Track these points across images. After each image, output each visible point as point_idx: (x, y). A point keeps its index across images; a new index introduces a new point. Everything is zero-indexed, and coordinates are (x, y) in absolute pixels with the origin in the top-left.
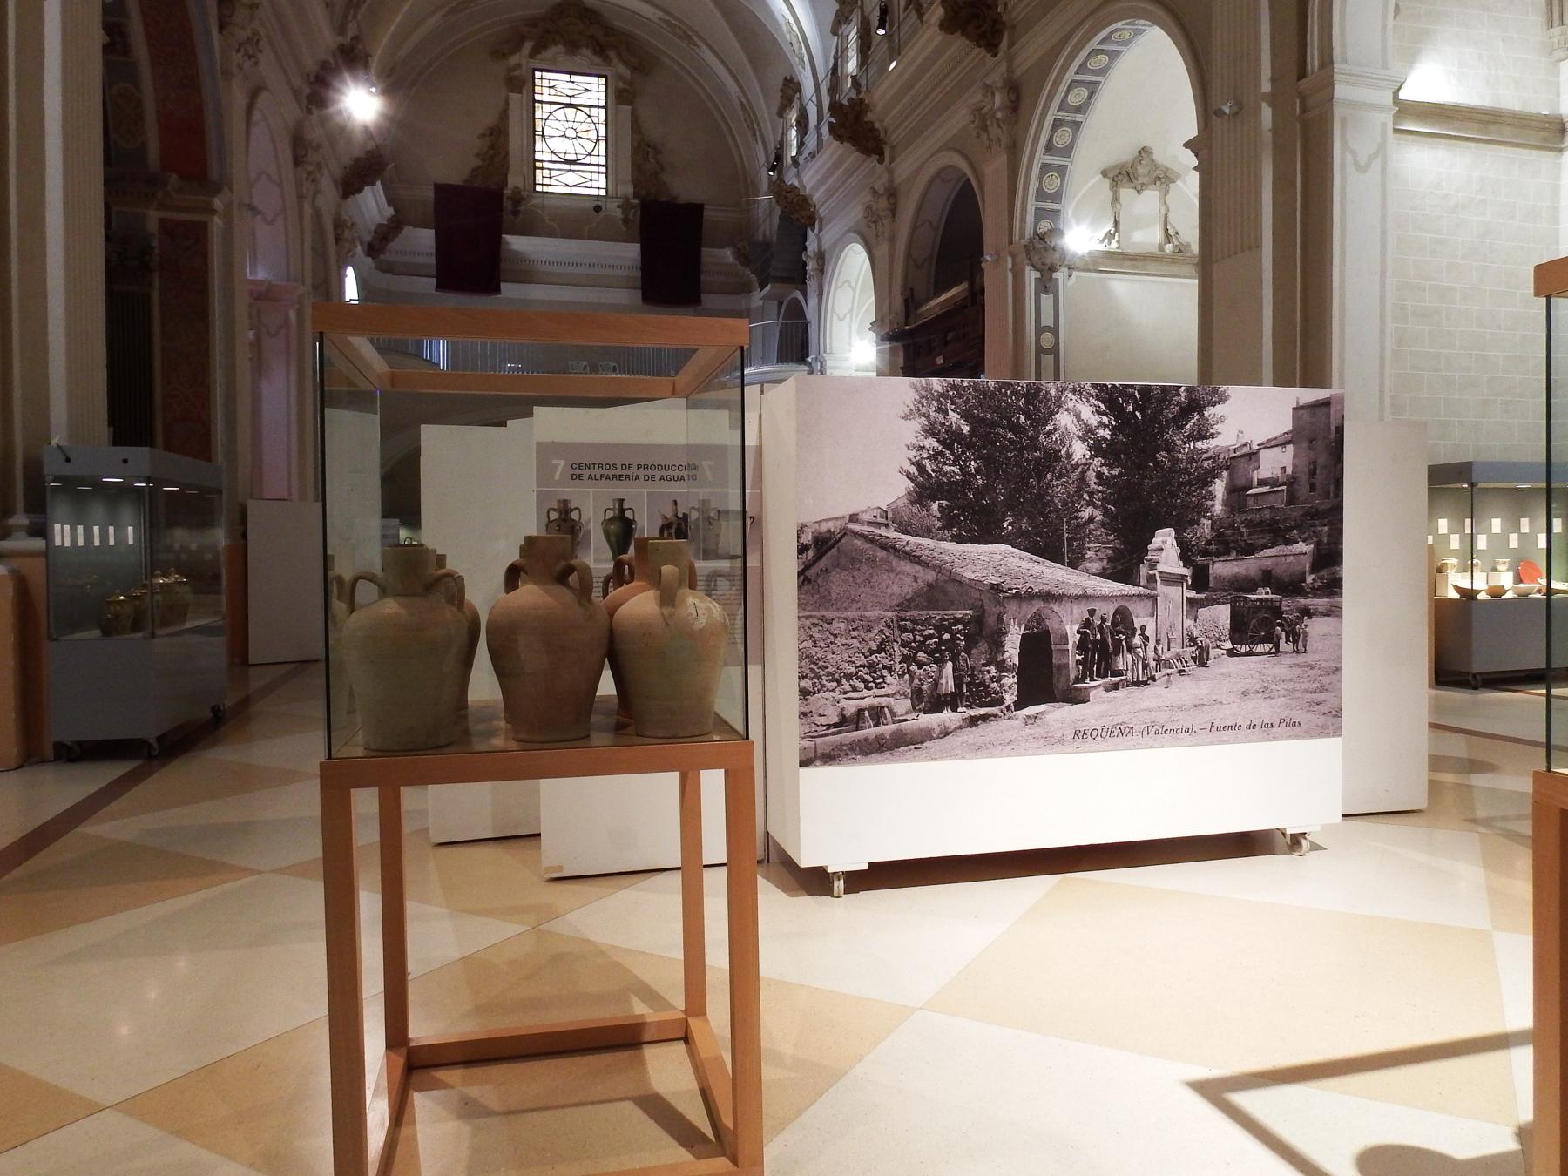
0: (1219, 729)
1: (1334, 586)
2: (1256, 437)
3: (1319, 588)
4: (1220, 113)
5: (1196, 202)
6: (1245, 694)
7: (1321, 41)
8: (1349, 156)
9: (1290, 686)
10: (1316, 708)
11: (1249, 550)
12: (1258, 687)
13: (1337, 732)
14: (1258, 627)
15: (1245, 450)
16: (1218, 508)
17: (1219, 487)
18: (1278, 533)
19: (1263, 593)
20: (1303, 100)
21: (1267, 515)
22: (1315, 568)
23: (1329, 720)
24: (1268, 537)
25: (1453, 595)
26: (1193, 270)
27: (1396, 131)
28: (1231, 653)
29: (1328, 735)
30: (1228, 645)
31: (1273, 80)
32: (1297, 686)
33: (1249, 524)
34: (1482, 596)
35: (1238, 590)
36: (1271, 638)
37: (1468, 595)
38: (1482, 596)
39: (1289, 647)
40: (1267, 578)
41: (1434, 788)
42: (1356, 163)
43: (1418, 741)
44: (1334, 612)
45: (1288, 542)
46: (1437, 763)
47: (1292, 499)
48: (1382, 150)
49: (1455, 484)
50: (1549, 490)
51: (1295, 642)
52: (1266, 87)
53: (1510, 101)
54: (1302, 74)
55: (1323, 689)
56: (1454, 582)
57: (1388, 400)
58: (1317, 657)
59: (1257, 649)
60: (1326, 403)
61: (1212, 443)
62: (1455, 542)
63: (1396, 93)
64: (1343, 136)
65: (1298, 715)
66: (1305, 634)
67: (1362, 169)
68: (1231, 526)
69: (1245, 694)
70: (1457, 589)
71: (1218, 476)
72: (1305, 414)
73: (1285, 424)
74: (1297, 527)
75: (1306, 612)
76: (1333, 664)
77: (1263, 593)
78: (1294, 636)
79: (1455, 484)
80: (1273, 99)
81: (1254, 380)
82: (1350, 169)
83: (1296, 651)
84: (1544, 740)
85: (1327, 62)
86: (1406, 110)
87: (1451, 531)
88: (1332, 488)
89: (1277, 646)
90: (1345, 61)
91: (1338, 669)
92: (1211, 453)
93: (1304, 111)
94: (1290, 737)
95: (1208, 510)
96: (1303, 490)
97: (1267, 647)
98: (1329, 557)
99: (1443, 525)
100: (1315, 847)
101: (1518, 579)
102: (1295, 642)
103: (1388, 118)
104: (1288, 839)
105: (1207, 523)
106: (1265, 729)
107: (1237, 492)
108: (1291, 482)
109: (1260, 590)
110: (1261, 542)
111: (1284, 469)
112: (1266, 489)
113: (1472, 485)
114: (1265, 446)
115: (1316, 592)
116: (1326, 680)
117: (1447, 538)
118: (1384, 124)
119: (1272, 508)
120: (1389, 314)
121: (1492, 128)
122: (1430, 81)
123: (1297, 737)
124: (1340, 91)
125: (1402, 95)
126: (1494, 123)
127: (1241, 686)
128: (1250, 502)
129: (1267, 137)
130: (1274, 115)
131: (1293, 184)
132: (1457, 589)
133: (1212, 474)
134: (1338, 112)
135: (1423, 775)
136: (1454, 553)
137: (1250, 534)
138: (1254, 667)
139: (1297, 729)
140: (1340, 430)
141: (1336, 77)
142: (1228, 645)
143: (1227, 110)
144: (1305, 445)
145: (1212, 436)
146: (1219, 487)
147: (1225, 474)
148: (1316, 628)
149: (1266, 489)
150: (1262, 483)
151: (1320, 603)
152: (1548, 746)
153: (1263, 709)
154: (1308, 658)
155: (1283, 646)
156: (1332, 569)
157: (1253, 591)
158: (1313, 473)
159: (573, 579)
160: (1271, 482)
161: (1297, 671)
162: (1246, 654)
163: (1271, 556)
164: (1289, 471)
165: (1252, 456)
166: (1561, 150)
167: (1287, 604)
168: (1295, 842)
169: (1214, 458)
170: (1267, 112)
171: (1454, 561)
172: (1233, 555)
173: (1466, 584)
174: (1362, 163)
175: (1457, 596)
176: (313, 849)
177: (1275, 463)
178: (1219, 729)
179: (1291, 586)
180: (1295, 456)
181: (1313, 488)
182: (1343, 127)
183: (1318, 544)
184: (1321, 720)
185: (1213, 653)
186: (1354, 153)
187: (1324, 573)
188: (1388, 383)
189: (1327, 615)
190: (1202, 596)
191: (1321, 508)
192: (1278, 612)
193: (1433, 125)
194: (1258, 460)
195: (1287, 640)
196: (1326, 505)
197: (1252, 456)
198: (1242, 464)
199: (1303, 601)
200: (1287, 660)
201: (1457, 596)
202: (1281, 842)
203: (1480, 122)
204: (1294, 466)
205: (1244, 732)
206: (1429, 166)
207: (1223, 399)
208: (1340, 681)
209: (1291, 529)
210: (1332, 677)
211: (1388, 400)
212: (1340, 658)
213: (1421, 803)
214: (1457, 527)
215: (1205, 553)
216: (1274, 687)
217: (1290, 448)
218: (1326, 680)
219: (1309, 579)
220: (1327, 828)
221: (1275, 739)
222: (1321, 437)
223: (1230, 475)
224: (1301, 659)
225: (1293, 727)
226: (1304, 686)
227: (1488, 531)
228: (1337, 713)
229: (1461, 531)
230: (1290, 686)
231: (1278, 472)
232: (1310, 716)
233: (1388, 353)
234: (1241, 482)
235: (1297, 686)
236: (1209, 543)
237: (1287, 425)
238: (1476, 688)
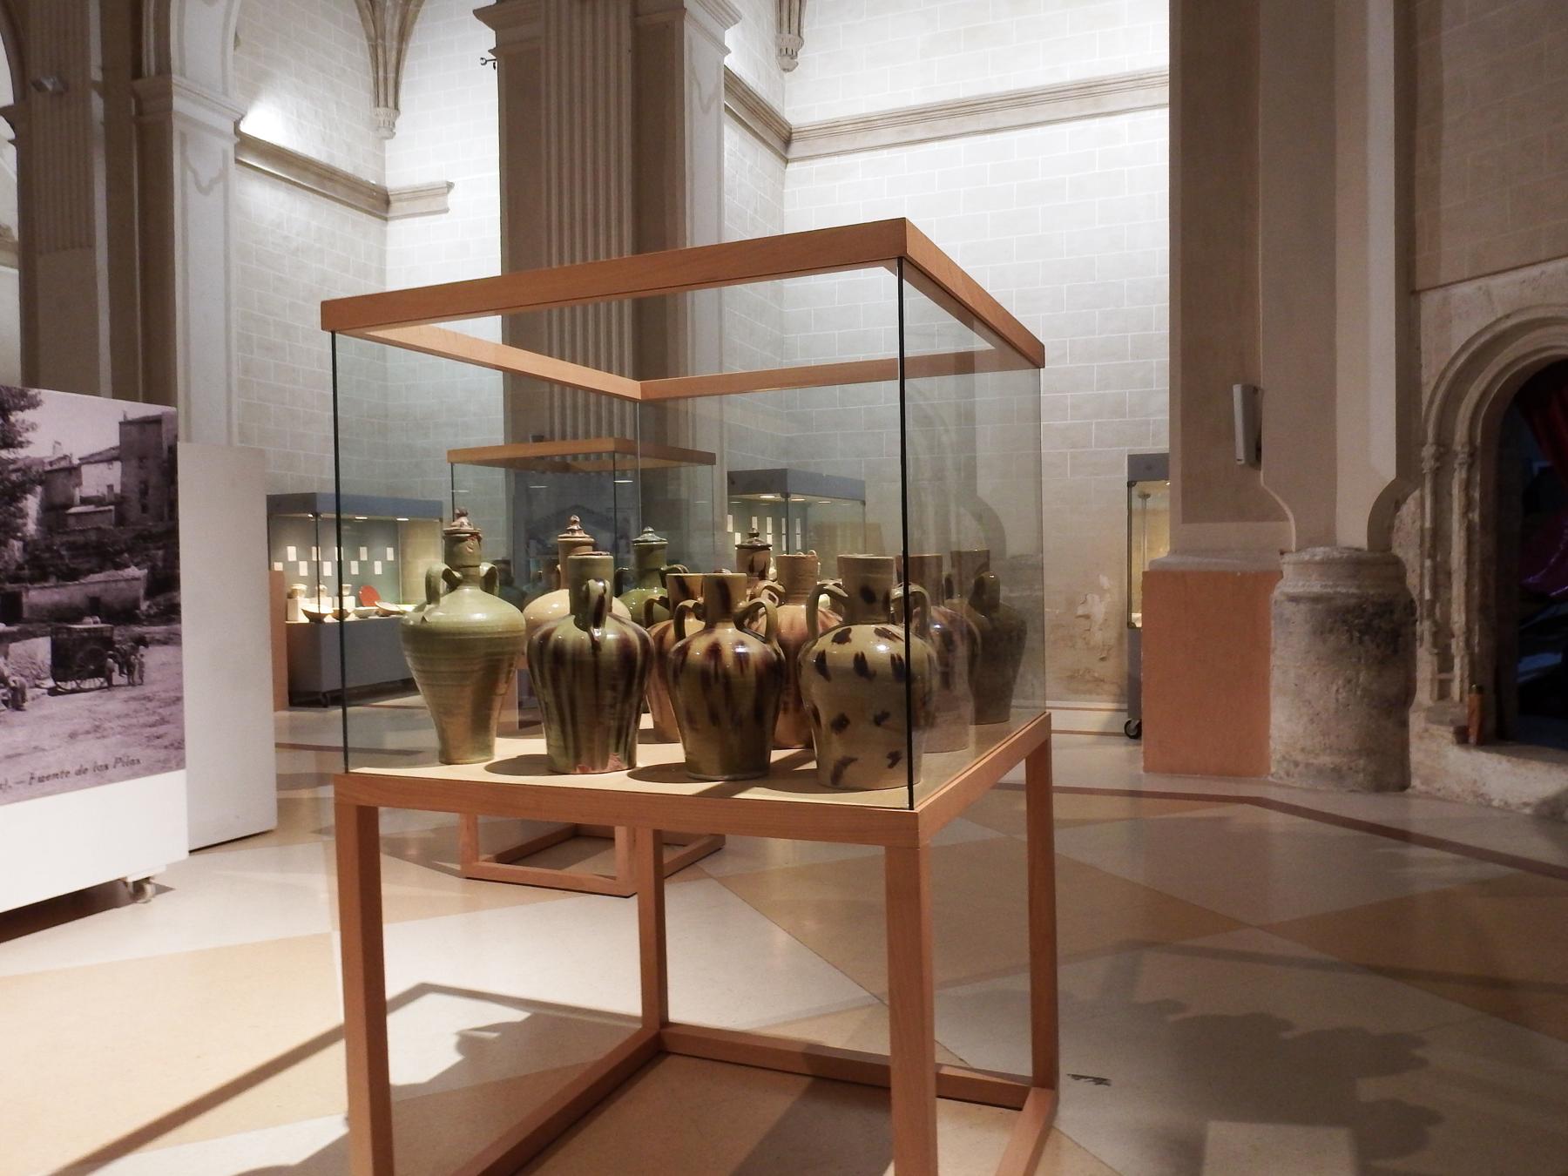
0: (41, 780)
1: (171, 613)
2: (77, 449)
3: (155, 615)
4: (40, 87)
5: (15, 178)
6: (73, 736)
7: (157, 48)
8: (189, 174)
9: (126, 722)
10: (157, 742)
11: (72, 575)
12: (87, 727)
13: (180, 764)
14: (79, 662)
15: (63, 464)
16: (31, 527)
17: (32, 504)
18: (105, 555)
19: (90, 623)
20: (139, 103)
21: (93, 536)
22: (149, 594)
23: (171, 753)
24: (94, 562)
25: (304, 620)
26: (14, 259)
27: (238, 162)
28: (53, 692)
29: (171, 769)
30: (50, 683)
31: (104, 69)
32: (134, 721)
33: (71, 546)
34: (329, 619)
35: (59, 620)
36: (102, 672)
37: (316, 619)
38: (329, 619)
39: (124, 680)
40: (95, 606)
41: (286, 809)
42: (198, 183)
43: (264, 763)
44: (173, 640)
45: (119, 567)
46: (286, 782)
47: (121, 520)
48: (223, 176)
49: (288, 513)
50: (339, 521)
51: (130, 673)
52: (96, 75)
53: (343, 163)
54: (137, 73)
55: (163, 721)
56: (304, 607)
57: (235, 429)
58: (155, 688)
59: (87, 684)
60: (157, 421)
61: (21, 453)
62: (303, 569)
63: (237, 124)
64: (183, 153)
65: (136, 752)
66: (142, 665)
67: (205, 191)
68: (49, 548)
69: (73, 736)
70: (307, 614)
71: (31, 491)
72: (134, 430)
73: (111, 439)
74: (130, 550)
75: (142, 641)
76: (172, 694)
77: (90, 623)
78: (128, 667)
79: (288, 513)
80: (105, 92)
81: (88, 386)
82: (191, 189)
83: (132, 684)
84: (341, 744)
85: (164, 69)
86: (247, 144)
87: (299, 558)
88: (166, 510)
89: (109, 680)
90: (183, 74)
91: (179, 699)
92: (20, 464)
93: (140, 112)
94: (128, 777)
95: (18, 529)
96: (134, 512)
97: (98, 682)
98: (165, 582)
99: (292, 552)
100: (161, 890)
101: (359, 603)
102: (130, 673)
103: (229, 146)
104: (131, 888)
105: (17, 544)
106: (98, 773)
107: (54, 511)
108: (120, 501)
109: (88, 620)
110: (87, 566)
111: (110, 487)
112: (91, 508)
113: (316, 515)
114: (89, 460)
115: (151, 619)
116: (165, 712)
117: (295, 565)
118: (225, 153)
119: (98, 529)
120: (234, 343)
121: (329, 184)
122: (267, 121)
123: (136, 775)
124: (178, 103)
125: (245, 128)
126: (331, 180)
127: (68, 728)
128: (71, 521)
129: (99, 129)
130: (106, 110)
131: (131, 187)
132: (307, 614)
133: (22, 489)
134: (177, 126)
135: (270, 796)
136: (302, 580)
137: (73, 557)
138: (84, 704)
139: (136, 767)
140: (173, 450)
141: (174, 88)
142: (50, 683)
143: (50, 87)
144: (134, 463)
145: (21, 445)
146: (32, 504)
147: (39, 489)
148: (153, 657)
149: (91, 508)
150: (85, 501)
151: (158, 630)
152: (345, 749)
153: (95, 751)
154: (146, 690)
155: (117, 678)
156: (169, 595)
157: (78, 620)
158: (144, 493)
159: (762, 623)
160: (98, 501)
161: (134, 705)
162: (73, 691)
163: (96, 582)
164: (117, 489)
165: (72, 471)
166: (386, 219)
167: (118, 633)
168: (138, 890)
169: (25, 470)
170: (97, 104)
171: (301, 587)
172: (53, 581)
173: (313, 609)
174: (204, 184)
175: (306, 620)
176: (1061, 808)
177: (99, 481)
178: (41, 780)
179: (125, 614)
180: (124, 473)
181: (144, 509)
182: (183, 143)
183: (152, 569)
184: (162, 754)
185: (29, 693)
186: (194, 172)
187: (160, 599)
188: (235, 410)
189: (165, 642)
190: (14, 629)
191: (154, 530)
192: (109, 643)
193: (273, 166)
194: (79, 477)
195: (121, 672)
196: (159, 528)
197: (72, 471)
198: (60, 480)
199: (137, 630)
200: (121, 694)
201: (306, 620)
202: (124, 892)
203: (318, 175)
204: (123, 484)
205: (73, 779)
206: (268, 203)
207: (34, 404)
208: (182, 711)
209: (121, 552)
210: (173, 708)
211: (235, 429)
212: (180, 688)
213: (270, 822)
214: (304, 554)
215: (16, 579)
216: (107, 725)
217: (117, 465)
218: (165, 712)
219: (144, 606)
220: (173, 868)
221: (111, 781)
222: (152, 458)
223: (47, 492)
224: (136, 692)
225: (130, 767)
226: (142, 721)
227: (383, 558)
228: (179, 745)
229: (309, 560)
230: (126, 722)
231: (105, 491)
232: (149, 752)
233: (234, 382)
234: (59, 499)
235: (134, 721)
236: (20, 567)
237: (115, 441)
238: (325, 706)
